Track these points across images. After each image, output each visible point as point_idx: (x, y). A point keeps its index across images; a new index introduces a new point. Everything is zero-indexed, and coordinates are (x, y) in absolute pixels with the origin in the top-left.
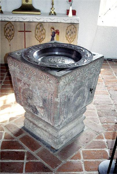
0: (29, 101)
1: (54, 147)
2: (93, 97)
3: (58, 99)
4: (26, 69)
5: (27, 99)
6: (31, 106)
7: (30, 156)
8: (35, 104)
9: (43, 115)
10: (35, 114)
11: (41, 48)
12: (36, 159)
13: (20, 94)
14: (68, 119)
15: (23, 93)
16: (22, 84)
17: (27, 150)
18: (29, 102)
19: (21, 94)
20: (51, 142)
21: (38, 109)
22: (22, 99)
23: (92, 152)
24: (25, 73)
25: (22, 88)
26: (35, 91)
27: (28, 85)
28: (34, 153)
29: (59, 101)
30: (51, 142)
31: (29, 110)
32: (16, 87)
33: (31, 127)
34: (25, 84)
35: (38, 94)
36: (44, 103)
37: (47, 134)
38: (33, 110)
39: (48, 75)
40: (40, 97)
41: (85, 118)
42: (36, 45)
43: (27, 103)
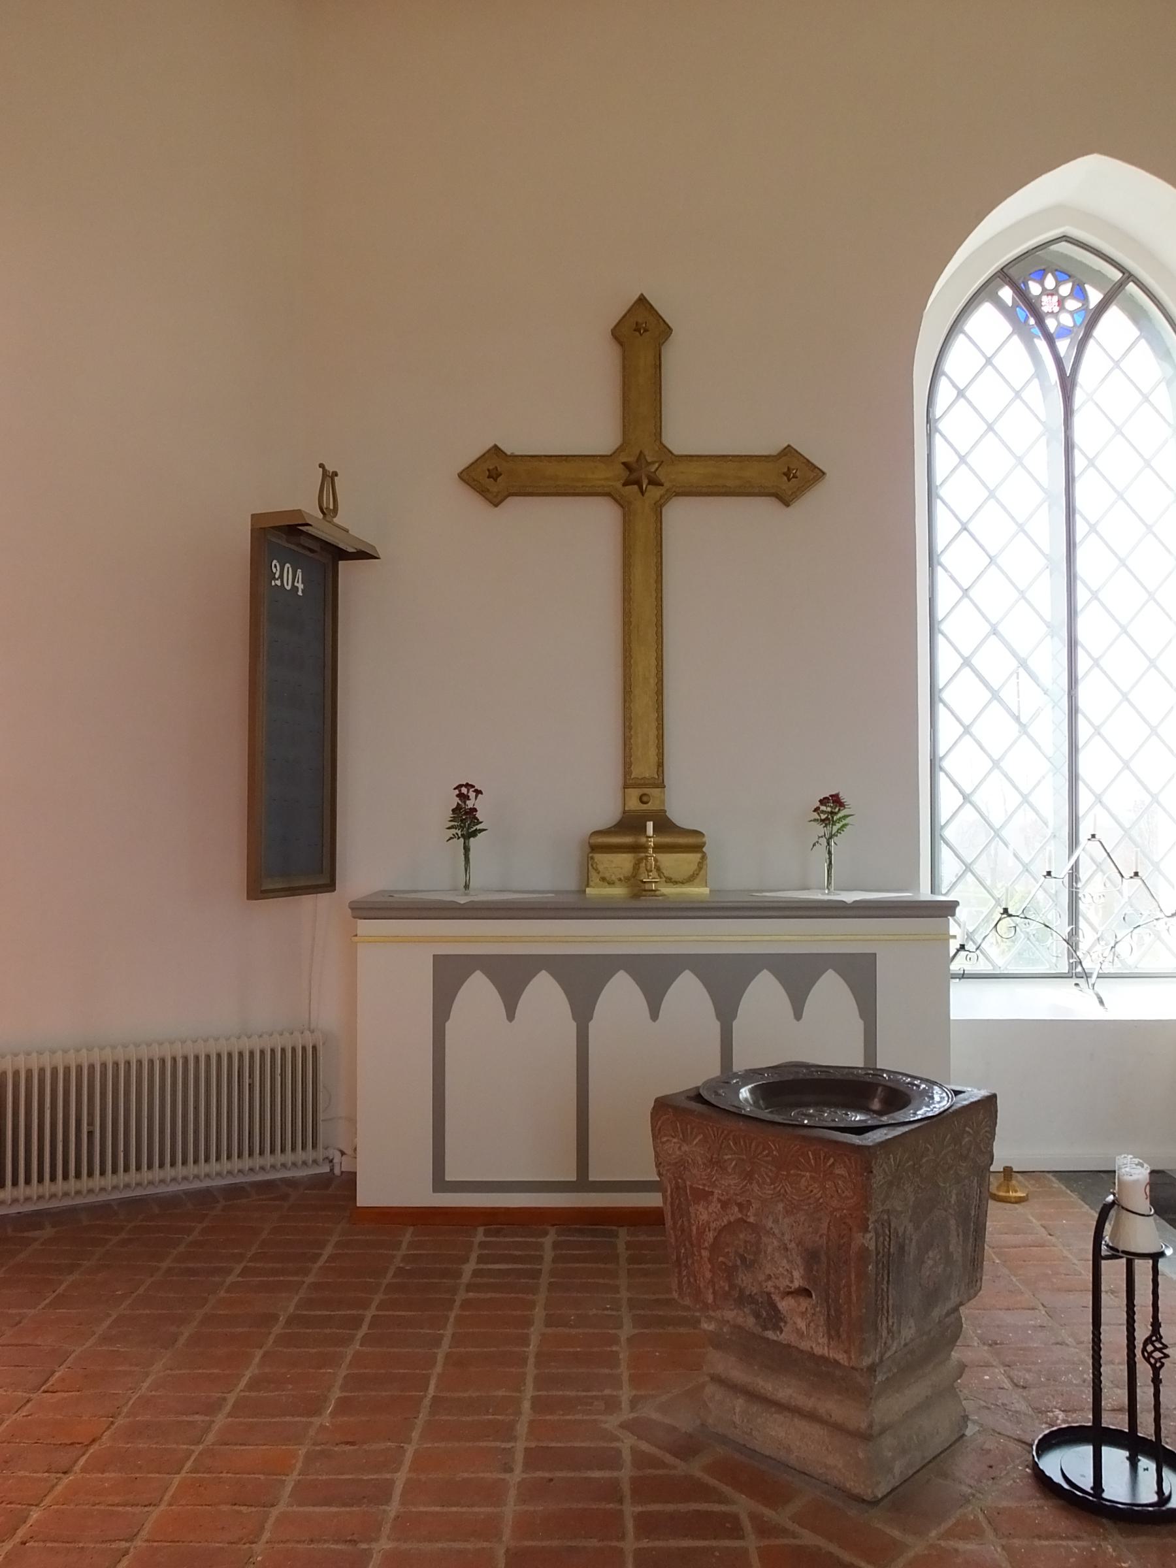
0: (744, 1279)
1: (858, 1489)
2: (982, 1270)
3: (868, 1236)
4: (735, 1144)
5: (730, 1272)
6: (751, 1299)
7: (764, 1529)
8: (770, 1283)
9: (804, 1328)
10: (770, 1334)
11: (767, 1078)
12: (794, 1536)
13: (700, 1255)
14: (903, 1342)
15: (715, 1247)
16: (715, 1207)
17: (742, 1505)
18: (739, 1282)
19: (705, 1253)
20: (840, 1466)
21: (784, 1305)
22: (708, 1275)
23: (1029, 1513)
24: (732, 1160)
25: (713, 1225)
26: (770, 1224)
27: (740, 1205)
28: (781, 1517)
29: (872, 1247)
30: (840, 1466)
31: (740, 1320)
32: (683, 1231)
33: (737, 1419)
34: (725, 1205)
35: (783, 1234)
36: (809, 1269)
37: (817, 1431)
38: (757, 1316)
39: (826, 1150)
40: (793, 1245)
41: (962, 1368)
42: (755, 1070)
43: (732, 1286)
